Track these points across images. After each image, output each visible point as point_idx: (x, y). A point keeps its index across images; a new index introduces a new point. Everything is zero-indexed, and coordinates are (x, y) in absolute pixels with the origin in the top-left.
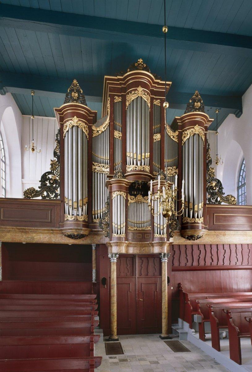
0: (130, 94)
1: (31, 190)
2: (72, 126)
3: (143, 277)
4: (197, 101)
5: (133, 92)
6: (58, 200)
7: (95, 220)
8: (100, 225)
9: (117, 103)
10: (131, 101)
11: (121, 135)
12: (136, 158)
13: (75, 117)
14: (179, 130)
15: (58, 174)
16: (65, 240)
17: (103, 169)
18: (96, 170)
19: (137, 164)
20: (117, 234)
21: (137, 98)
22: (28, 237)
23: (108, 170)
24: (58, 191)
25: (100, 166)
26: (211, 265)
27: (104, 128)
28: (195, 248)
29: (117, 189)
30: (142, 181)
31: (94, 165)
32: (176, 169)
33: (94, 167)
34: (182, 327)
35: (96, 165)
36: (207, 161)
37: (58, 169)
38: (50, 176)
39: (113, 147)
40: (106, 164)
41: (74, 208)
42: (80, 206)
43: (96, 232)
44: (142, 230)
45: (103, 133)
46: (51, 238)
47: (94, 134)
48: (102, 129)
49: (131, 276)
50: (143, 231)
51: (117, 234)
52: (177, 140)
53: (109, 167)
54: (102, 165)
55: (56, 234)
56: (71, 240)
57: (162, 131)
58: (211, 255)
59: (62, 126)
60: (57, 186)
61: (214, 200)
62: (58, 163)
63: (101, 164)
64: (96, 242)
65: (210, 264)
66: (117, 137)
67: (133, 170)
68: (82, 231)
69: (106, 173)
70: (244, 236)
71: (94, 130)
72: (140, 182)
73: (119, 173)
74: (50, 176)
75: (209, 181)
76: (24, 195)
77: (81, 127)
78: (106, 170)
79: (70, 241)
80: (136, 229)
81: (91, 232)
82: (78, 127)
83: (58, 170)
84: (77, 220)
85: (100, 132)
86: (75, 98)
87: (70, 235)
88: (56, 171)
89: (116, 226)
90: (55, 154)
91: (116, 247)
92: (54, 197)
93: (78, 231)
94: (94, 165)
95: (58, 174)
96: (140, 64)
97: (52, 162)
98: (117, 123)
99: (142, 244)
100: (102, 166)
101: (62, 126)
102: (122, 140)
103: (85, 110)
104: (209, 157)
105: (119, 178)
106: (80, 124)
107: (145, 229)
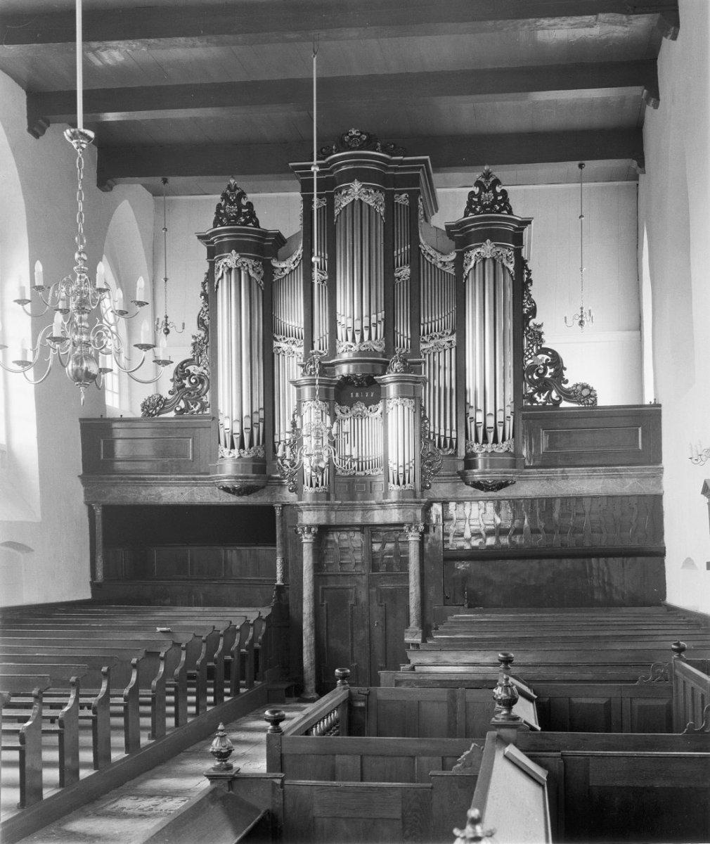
5: (344, 192)
11: (327, 278)
17: (294, 347)
22: (150, 495)
23: (302, 350)
24: (207, 398)
31: (277, 340)
32: (452, 334)
33: (276, 344)
35: (281, 339)
36: (526, 309)
38: (191, 368)
46: (192, 494)
52: (453, 270)
53: (303, 344)
55: (202, 486)
74: (191, 368)
75: (530, 354)
76: (143, 410)
79: (233, 499)
85: (287, 271)
86: (232, 215)
90: (201, 322)
91: (307, 512)
92: (198, 411)
96: (354, 136)
97: (193, 341)
106: (244, 263)
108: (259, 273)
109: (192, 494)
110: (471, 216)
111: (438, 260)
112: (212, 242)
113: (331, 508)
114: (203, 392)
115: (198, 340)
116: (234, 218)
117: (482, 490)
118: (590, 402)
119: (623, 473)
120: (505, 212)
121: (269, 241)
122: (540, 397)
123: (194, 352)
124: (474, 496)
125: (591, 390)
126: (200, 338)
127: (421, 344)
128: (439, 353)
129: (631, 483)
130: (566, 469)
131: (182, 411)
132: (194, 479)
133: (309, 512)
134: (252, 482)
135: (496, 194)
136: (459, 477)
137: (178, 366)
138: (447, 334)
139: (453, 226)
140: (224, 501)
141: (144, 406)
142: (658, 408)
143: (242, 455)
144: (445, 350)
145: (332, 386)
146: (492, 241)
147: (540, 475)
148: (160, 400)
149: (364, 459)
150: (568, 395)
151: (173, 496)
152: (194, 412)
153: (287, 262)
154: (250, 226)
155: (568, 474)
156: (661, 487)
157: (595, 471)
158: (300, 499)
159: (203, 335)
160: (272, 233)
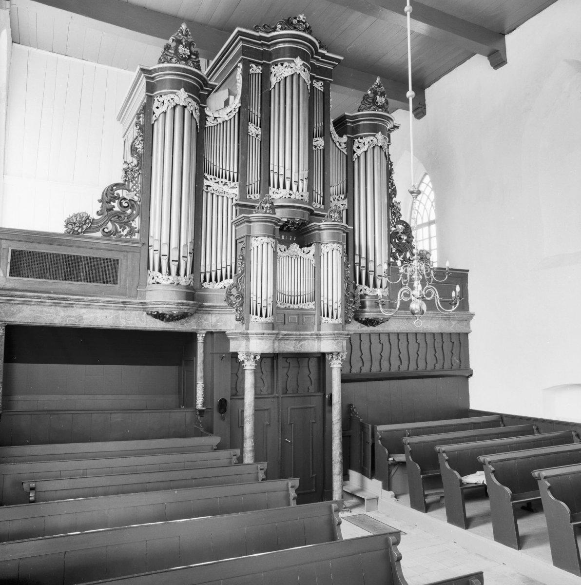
0: (279, 65)
1: (81, 218)
2: (175, 105)
3: (290, 395)
4: (379, 93)
6: (134, 242)
7: (205, 285)
8: (227, 297)
10: (282, 78)
11: (260, 133)
12: (283, 173)
14: (348, 135)
16: (147, 322)
17: (225, 188)
18: (211, 188)
19: (291, 189)
20: (261, 316)
21: (292, 75)
23: (236, 191)
24: (136, 223)
25: (218, 182)
26: (380, 371)
27: (227, 115)
28: (375, 339)
29: (262, 233)
30: (300, 220)
31: (207, 179)
33: (206, 183)
34: (360, 488)
35: (211, 179)
38: (121, 193)
40: (230, 180)
42: (183, 257)
43: (210, 309)
44: (298, 309)
45: (225, 123)
46: (117, 317)
47: (207, 123)
49: (268, 394)
50: (300, 310)
51: (261, 316)
54: (224, 180)
56: (158, 323)
57: (325, 134)
58: (360, 354)
59: (150, 99)
60: (134, 212)
62: (137, 168)
64: (209, 328)
65: (397, 368)
66: (253, 135)
67: (285, 197)
68: (188, 307)
70: (445, 320)
71: (208, 116)
72: (297, 221)
74: (120, 192)
75: (393, 223)
76: (66, 226)
78: (231, 191)
81: (199, 309)
82: (184, 107)
84: (178, 284)
85: (220, 121)
86: (184, 56)
90: (133, 149)
91: (258, 341)
92: (126, 235)
93: (181, 307)
94: (207, 179)
95: (137, 190)
97: (125, 166)
98: (254, 110)
99: (300, 335)
100: (222, 182)
101: (150, 99)
103: (194, 77)
106: (190, 103)
107: (304, 307)
109: (117, 317)
112: (153, 78)
113: (277, 338)
115: (130, 167)
122: (400, 256)
129: (454, 324)
131: (109, 234)
132: (124, 303)
133: (261, 341)
134: (184, 309)
137: (109, 187)
140: (151, 326)
141: (68, 223)
148: (88, 219)
149: (302, 294)
152: (122, 235)
156: (470, 328)
158: (247, 329)
159: (135, 162)
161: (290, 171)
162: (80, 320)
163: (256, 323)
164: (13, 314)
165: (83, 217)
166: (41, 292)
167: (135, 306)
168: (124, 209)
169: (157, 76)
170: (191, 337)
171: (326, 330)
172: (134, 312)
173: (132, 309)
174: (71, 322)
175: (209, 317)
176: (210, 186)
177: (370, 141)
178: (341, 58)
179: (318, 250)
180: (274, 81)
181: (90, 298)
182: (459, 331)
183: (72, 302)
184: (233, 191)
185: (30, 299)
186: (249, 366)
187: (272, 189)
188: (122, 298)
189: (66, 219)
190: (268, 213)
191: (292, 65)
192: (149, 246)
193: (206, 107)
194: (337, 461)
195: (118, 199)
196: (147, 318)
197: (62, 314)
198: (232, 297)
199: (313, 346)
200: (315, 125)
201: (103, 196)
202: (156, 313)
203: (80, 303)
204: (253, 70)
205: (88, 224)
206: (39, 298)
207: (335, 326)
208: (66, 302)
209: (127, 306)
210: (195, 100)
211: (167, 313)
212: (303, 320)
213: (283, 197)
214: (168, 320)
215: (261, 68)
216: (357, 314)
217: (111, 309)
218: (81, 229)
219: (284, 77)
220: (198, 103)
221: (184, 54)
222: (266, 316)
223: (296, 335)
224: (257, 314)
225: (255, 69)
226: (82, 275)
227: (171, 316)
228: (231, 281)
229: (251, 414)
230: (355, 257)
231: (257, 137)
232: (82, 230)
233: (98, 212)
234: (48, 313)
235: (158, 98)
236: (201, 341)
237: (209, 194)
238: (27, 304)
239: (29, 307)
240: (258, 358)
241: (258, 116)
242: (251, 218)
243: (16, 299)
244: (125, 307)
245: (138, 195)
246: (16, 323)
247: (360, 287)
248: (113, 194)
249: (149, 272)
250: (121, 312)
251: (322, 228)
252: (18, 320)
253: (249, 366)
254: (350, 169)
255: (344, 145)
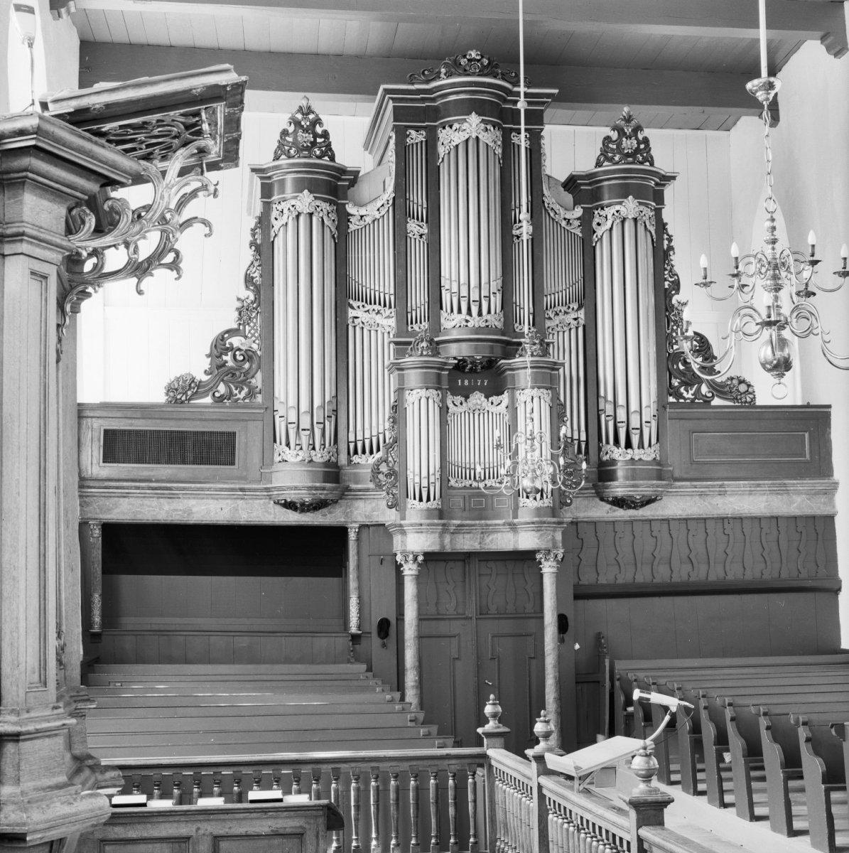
1: (185, 381)
2: (297, 213)
8: (373, 476)
9: (415, 146)
11: (426, 231)
12: (466, 295)
13: (304, 192)
15: (256, 335)
16: (275, 514)
17: (378, 319)
20: (421, 500)
21: (467, 141)
22: (177, 510)
23: (392, 322)
24: (257, 381)
25: (368, 311)
27: (378, 210)
30: (483, 357)
31: (353, 308)
32: (580, 308)
33: (351, 313)
35: (359, 307)
36: (667, 283)
37: (255, 320)
38: (236, 341)
39: (403, 249)
40: (385, 306)
41: (303, 430)
42: (317, 423)
45: (376, 223)
47: (351, 226)
48: (371, 212)
51: (421, 500)
52: (579, 230)
54: (377, 307)
59: (267, 207)
60: (254, 366)
61: (691, 392)
62: (255, 305)
63: (371, 304)
66: (415, 237)
67: (460, 326)
68: (325, 492)
69: (388, 329)
71: (352, 215)
73: (422, 341)
74: (236, 341)
76: (167, 394)
77: (321, 215)
78: (385, 322)
79: (292, 518)
80: (471, 485)
83: (255, 325)
84: (311, 461)
85: (368, 220)
86: (305, 145)
87: (291, 502)
88: (249, 326)
89: (417, 480)
90: (249, 280)
91: (416, 535)
92: (244, 399)
93: (314, 492)
94: (353, 308)
95: (256, 335)
96: (474, 60)
97: (239, 304)
99: (487, 525)
100: (374, 310)
101: (267, 207)
102: (428, 244)
104: (671, 271)
105: (422, 355)
106: (318, 207)
107: (494, 485)
108: (334, 220)
110: (607, 166)
111: (562, 216)
112: (269, 178)
114: (252, 374)
115: (245, 304)
116: (307, 149)
117: (622, 507)
118: (748, 400)
119: (792, 488)
120: (648, 164)
121: (345, 180)
122: (687, 391)
123: (240, 319)
124: (610, 515)
125: (749, 386)
126: (249, 302)
127: (547, 321)
128: (564, 332)
130: (725, 483)
131: (220, 400)
132: (242, 490)
133: (420, 534)
134: (322, 495)
135: (316, 135)
136: (594, 491)
138: (573, 309)
139: (582, 176)
140: (281, 520)
141: (170, 389)
142: (827, 410)
143: (314, 459)
144: (570, 329)
145: (447, 370)
146: (636, 198)
147: (693, 490)
148: (193, 381)
150: (719, 389)
151: (208, 512)
152: (239, 399)
153: (369, 207)
154: (326, 160)
155: (727, 489)
156: (834, 507)
157: (759, 485)
158: (403, 518)
159: (252, 297)
160: (351, 171)
161: (467, 286)
162: (188, 515)
163: (415, 510)
164: (109, 510)
165: (187, 380)
166: (140, 481)
167: (258, 493)
168: (239, 364)
169: (274, 174)
170: (340, 533)
171: (524, 517)
172: (258, 501)
173: (255, 497)
174: (177, 518)
175: (360, 504)
176: (357, 318)
177: (615, 213)
178: (556, 91)
179: (513, 400)
180: (441, 150)
181: (198, 485)
182: (808, 512)
183: (178, 492)
184: (387, 322)
185: (127, 491)
186: (410, 570)
187: (444, 314)
188: (239, 483)
189: (165, 384)
190: (425, 356)
191: (465, 126)
192: (274, 411)
193: (347, 203)
194: (551, 710)
195: (232, 350)
196: (274, 509)
197: (166, 507)
198: (381, 476)
199: (503, 541)
200: (513, 203)
201: (211, 348)
202: (283, 502)
203: (187, 492)
204: (412, 139)
205: (194, 388)
206: (138, 488)
207: (538, 511)
208: (170, 492)
209: (247, 493)
210: (325, 200)
211: (297, 501)
212: (470, 503)
213: (458, 326)
214: (302, 511)
215: (424, 133)
216: (599, 490)
217: (227, 499)
218: (184, 396)
219: (454, 145)
220: (331, 202)
221: (305, 142)
222: (428, 499)
223: (481, 525)
224: (415, 499)
225: (416, 137)
226: (190, 456)
227: (303, 504)
228: (378, 456)
229: (413, 636)
230: (600, 400)
231: (421, 238)
232: (186, 397)
233: (205, 371)
234: (149, 506)
235: (276, 205)
236: (353, 539)
237: (357, 328)
238: (124, 497)
239: (127, 500)
240: (420, 558)
241: (422, 206)
242: (402, 364)
243: (111, 490)
244: (245, 495)
245: (257, 342)
246: (114, 521)
247: (605, 448)
248: (225, 345)
249: (275, 446)
250: (240, 502)
251: (517, 367)
252: (115, 517)
253: (410, 570)
254: (588, 261)
255: (578, 223)
